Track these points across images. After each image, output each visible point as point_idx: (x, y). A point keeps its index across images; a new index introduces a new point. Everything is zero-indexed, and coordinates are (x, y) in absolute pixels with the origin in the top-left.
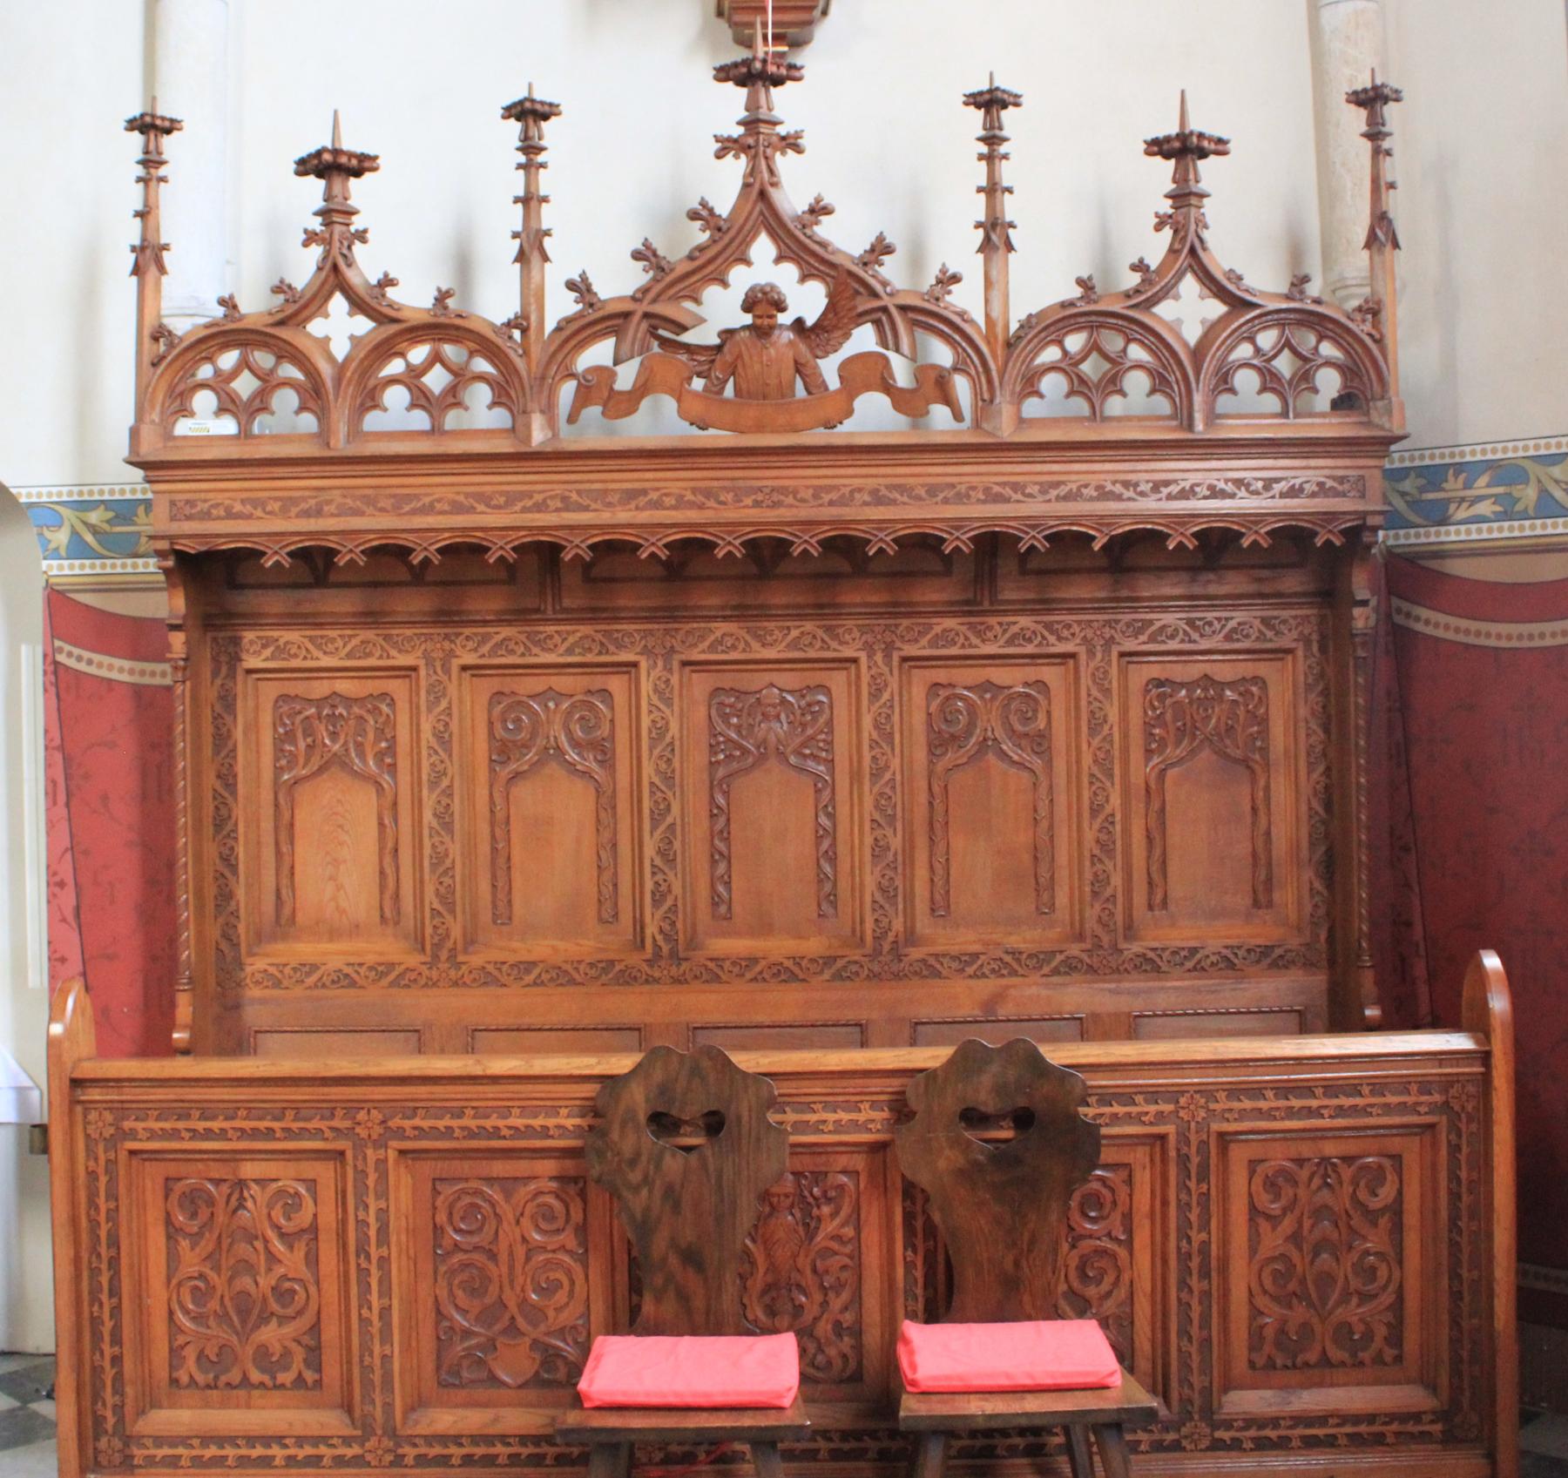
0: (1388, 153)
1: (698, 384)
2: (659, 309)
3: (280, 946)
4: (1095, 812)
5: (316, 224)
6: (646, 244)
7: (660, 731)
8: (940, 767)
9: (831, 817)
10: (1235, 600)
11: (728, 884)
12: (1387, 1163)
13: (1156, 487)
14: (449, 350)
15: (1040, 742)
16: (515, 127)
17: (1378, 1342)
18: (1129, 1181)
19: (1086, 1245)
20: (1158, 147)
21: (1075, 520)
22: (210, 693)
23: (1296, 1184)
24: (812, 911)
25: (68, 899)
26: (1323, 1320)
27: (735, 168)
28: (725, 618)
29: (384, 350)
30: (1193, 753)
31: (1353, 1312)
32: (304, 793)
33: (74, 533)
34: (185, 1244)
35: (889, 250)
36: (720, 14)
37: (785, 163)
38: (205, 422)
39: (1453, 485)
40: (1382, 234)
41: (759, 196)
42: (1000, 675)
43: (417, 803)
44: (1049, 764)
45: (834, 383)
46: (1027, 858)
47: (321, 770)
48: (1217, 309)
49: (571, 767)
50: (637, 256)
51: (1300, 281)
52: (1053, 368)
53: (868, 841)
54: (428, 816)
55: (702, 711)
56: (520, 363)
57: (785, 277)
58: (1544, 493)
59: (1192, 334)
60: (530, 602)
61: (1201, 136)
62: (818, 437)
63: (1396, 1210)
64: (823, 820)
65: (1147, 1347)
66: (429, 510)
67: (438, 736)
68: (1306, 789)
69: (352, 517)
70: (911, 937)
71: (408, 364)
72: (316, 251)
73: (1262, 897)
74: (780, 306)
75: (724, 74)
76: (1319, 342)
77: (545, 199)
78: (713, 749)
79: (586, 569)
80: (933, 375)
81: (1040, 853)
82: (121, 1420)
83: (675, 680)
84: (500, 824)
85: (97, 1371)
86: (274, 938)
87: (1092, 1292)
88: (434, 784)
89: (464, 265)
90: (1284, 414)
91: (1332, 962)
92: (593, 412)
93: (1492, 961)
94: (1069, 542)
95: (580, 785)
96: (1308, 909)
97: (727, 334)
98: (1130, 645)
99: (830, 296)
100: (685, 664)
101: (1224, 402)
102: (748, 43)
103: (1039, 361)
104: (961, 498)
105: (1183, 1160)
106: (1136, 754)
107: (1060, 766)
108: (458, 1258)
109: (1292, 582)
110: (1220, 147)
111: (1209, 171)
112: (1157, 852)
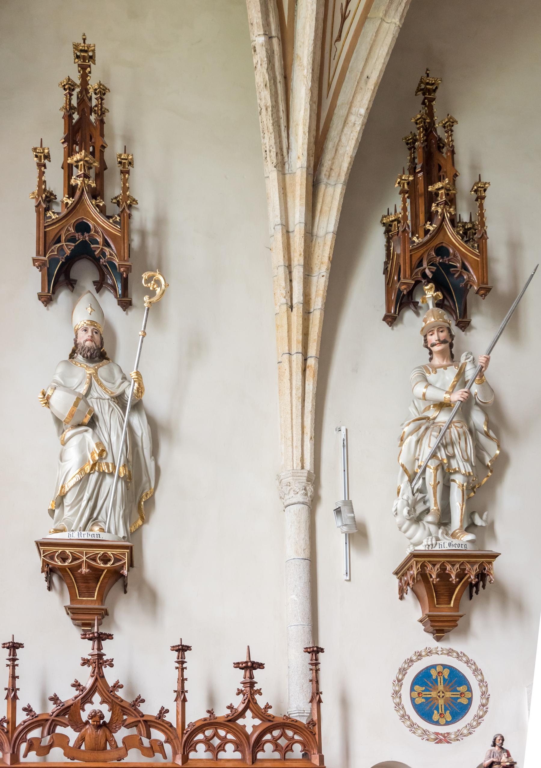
41: (99, 677)
45: (120, 745)
71: (205, 736)
76: (294, 734)
103: (196, 739)
110: (261, 666)
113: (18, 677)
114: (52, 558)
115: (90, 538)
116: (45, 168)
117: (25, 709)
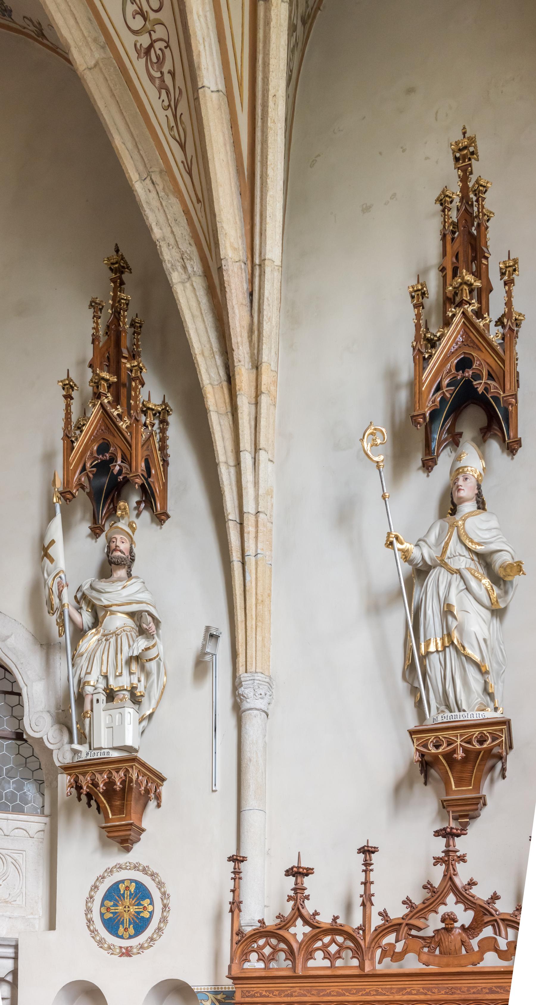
1: (426, 950)
5: (292, 893)
16: (362, 856)
27: (441, 868)
29: (314, 938)
33: (212, 1002)
38: (254, 964)
41: (449, 877)
45: (476, 949)
50: (404, 903)
56: (362, 943)
62: (470, 968)
66: (329, 995)
72: (292, 903)
74: (455, 920)
97: (437, 931)
114: (425, 746)
115: (445, 720)
116: (142, 387)
117: (380, 914)
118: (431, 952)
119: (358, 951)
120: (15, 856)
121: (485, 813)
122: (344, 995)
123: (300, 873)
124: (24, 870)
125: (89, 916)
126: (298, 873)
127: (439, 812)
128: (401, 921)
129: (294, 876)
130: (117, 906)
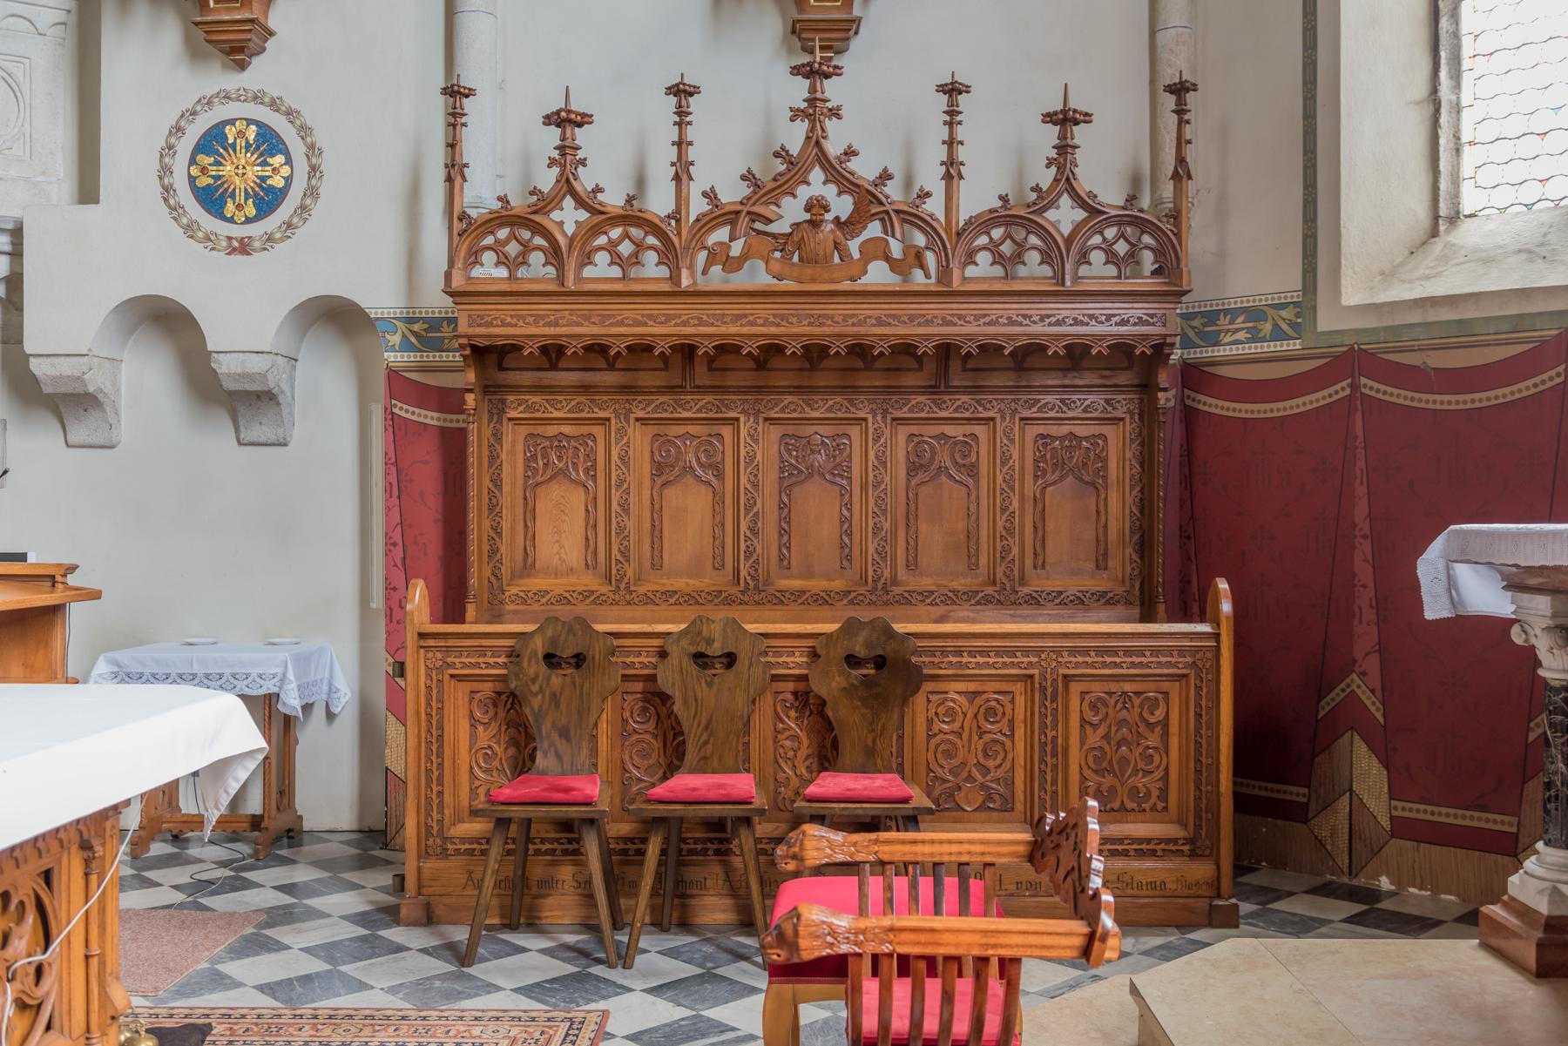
0: (1188, 122)
1: (778, 255)
2: (756, 209)
3: (525, 581)
4: (1003, 510)
5: (556, 154)
6: (749, 171)
7: (751, 458)
8: (914, 482)
9: (850, 510)
10: (1089, 388)
11: (789, 549)
12: (1160, 696)
13: (1042, 318)
14: (633, 231)
15: (972, 471)
16: (673, 100)
17: (1154, 799)
18: (1013, 701)
19: (988, 737)
20: (1049, 118)
21: (994, 336)
22: (487, 432)
23: (1107, 706)
24: (838, 566)
25: (398, 553)
26: (1122, 785)
27: (802, 127)
28: (790, 393)
29: (596, 230)
30: (1062, 478)
31: (1140, 781)
32: (541, 491)
33: (404, 335)
34: (481, 728)
35: (890, 177)
36: (793, 32)
37: (831, 125)
38: (489, 270)
39: (1224, 321)
40: (1182, 173)
41: (815, 141)
42: (950, 430)
43: (608, 499)
44: (977, 482)
45: (856, 255)
46: (963, 537)
47: (553, 477)
48: (1081, 214)
49: (698, 478)
50: (743, 178)
51: (1132, 199)
52: (984, 248)
53: (871, 524)
54: (615, 505)
55: (776, 448)
56: (675, 240)
57: (830, 192)
58: (1276, 326)
59: (1066, 229)
60: (678, 382)
61: (1075, 111)
62: (846, 285)
63: (1165, 723)
64: (845, 512)
65: (1022, 797)
66: (621, 324)
67: (621, 458)
68: (1129, 500)
69: (574, 326)
70: (894, 581)
72: (556, 170)
73: (1101, 565)
74: (826, 209)
75: (796, 71)
77: (690, 143)
78: (781, 470)
79: (710, 360)
80: (913, 251)
81: (971, 535)
82: (441, 830)
83: (760, 429)
84: (656, 510)
85: (429, 800)
86: (521, 576)
87: (991, 764)
88: (618, 486)
89: (641, 182)
90: (1119, 277)
91: (1142, 603)
92: (716, 269)
93: (1223, 585)
94: (989, 349)
95: (703, 488)
96: (1128, 570)
97: (797, 225)
98: (1026, 414)
99: (855, 203)
100: (766, 419)
101: (1084, 270)
102: (811, 52)
104: (929, 323)
105: (1043, 689)
106: (1029, 478)
107: (984, 483)
108: (635, 737)
109: (1124, 378)
110: (1087, 117)
111: (1080, 133)
112: (1040, 535)
113: (944, 142)
118: (787, 258)
119: (670, 254)
120: (9, 66)
121: (856, 44)
122: (646, 324)
123: (570, 121)
124: (27, 93)
125: (166, 181)
126: (565, 120)
127: (785, 39)
128: (739, 208)
129: (558, 126)
130: (221, 164)
